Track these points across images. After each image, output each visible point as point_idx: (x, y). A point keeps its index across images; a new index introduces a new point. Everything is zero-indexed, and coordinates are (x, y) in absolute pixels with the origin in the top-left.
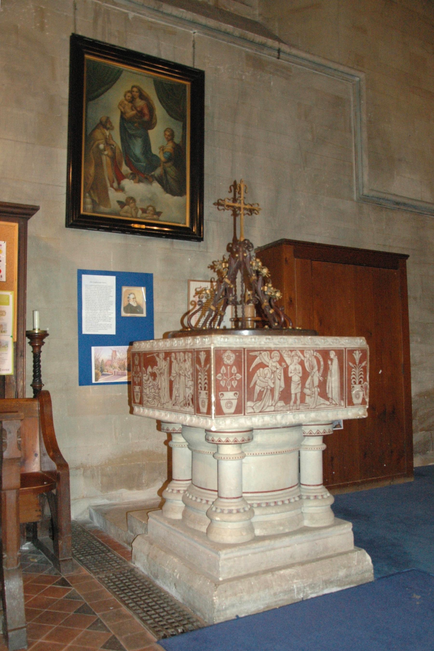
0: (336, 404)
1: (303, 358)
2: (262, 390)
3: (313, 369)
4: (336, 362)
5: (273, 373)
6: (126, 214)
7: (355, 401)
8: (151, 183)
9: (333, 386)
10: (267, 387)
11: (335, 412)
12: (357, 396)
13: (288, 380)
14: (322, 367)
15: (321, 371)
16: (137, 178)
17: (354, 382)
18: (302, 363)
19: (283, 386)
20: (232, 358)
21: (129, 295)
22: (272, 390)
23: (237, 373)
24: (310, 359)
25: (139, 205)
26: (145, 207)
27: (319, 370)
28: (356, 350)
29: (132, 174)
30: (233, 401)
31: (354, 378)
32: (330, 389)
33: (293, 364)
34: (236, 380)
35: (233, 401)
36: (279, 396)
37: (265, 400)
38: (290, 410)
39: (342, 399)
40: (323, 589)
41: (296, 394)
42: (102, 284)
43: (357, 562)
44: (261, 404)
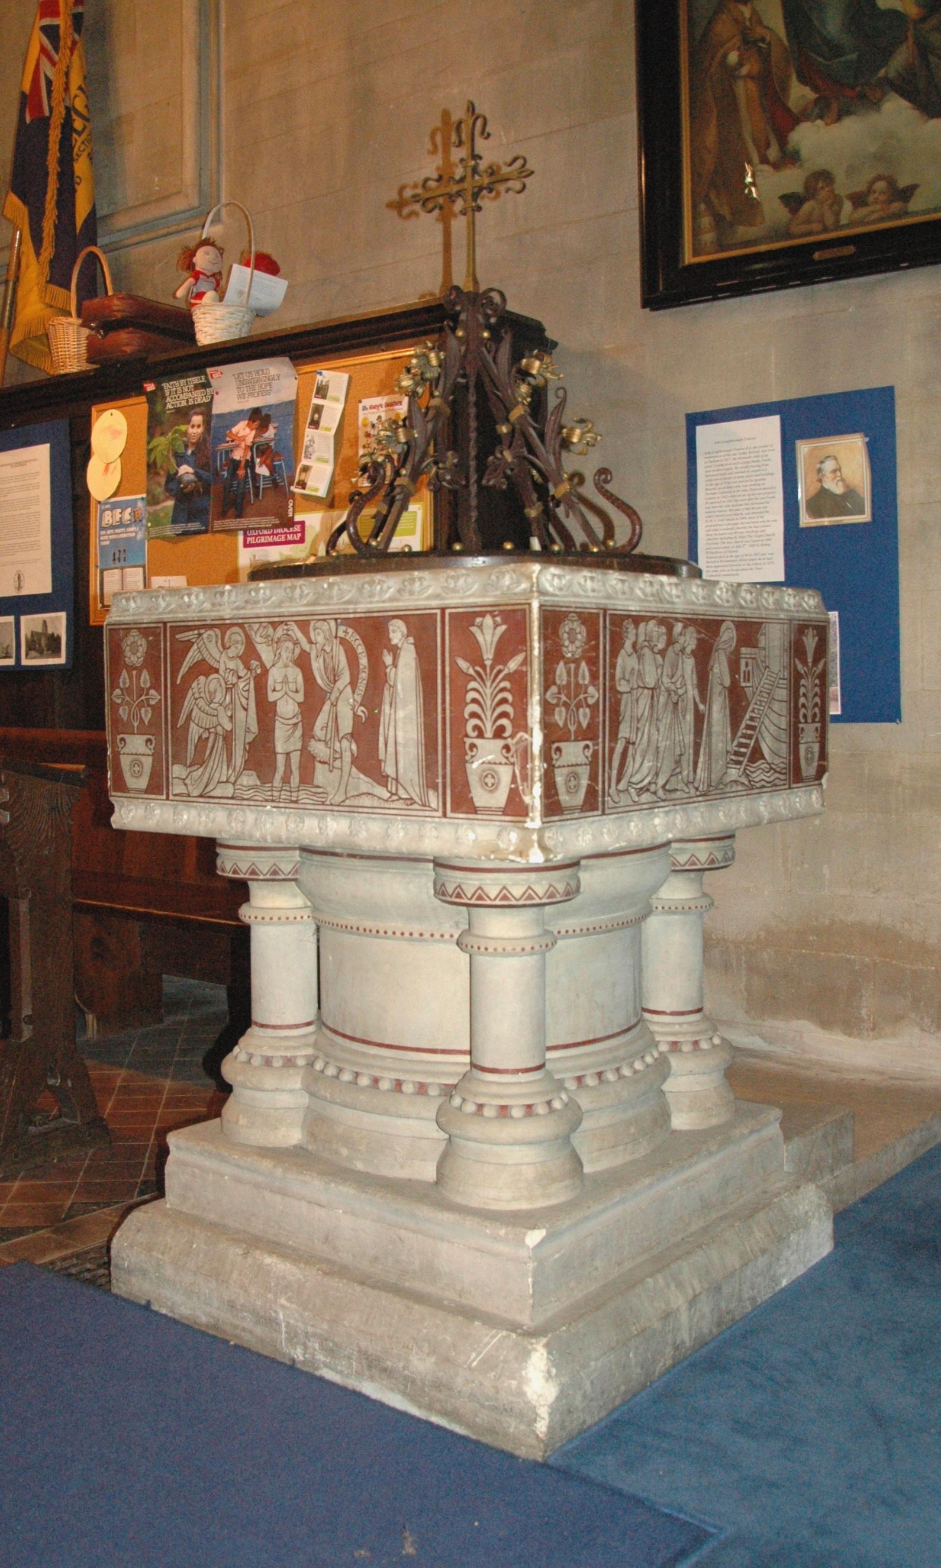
0: (411, 801)
1: (306, 647)
2: (205, 736)
3: (335, 681)
4: (408, 657)
5: (230, 689)
6: (813, 225)
7: (480, 797)
8: (876, 105)
9: (400, 740)
10: (215, 727)
11: (413, 828)
12: (489, 780)
13: (266, 711)
14: (364, 675)
15: (362, 687)
16: (835, 107)
17: (476, 728)
18: (303, 662)
19: (254, 728)
20: (141, 649)
21: (822, 462)
22: (228, 738)
23: (150, 688)
24: (327, 648)
25: (844, 186)
26: (859, 187)
27: (353, 684)
28: (482, 614)
29: (816, 102)
30: (143, 759)
31: (474, 715)
32: (391, 749)
33: (280, 664)
34: (149, 705)
35: (143, 759)
36: (243, 756)
37: (211, 763)
38: (273, 801)
39: (432, 785)
40: (359, 1374)
41: (288, 754)
42: (745, 444)
43: (483, 1361)
44: (203, 774)
